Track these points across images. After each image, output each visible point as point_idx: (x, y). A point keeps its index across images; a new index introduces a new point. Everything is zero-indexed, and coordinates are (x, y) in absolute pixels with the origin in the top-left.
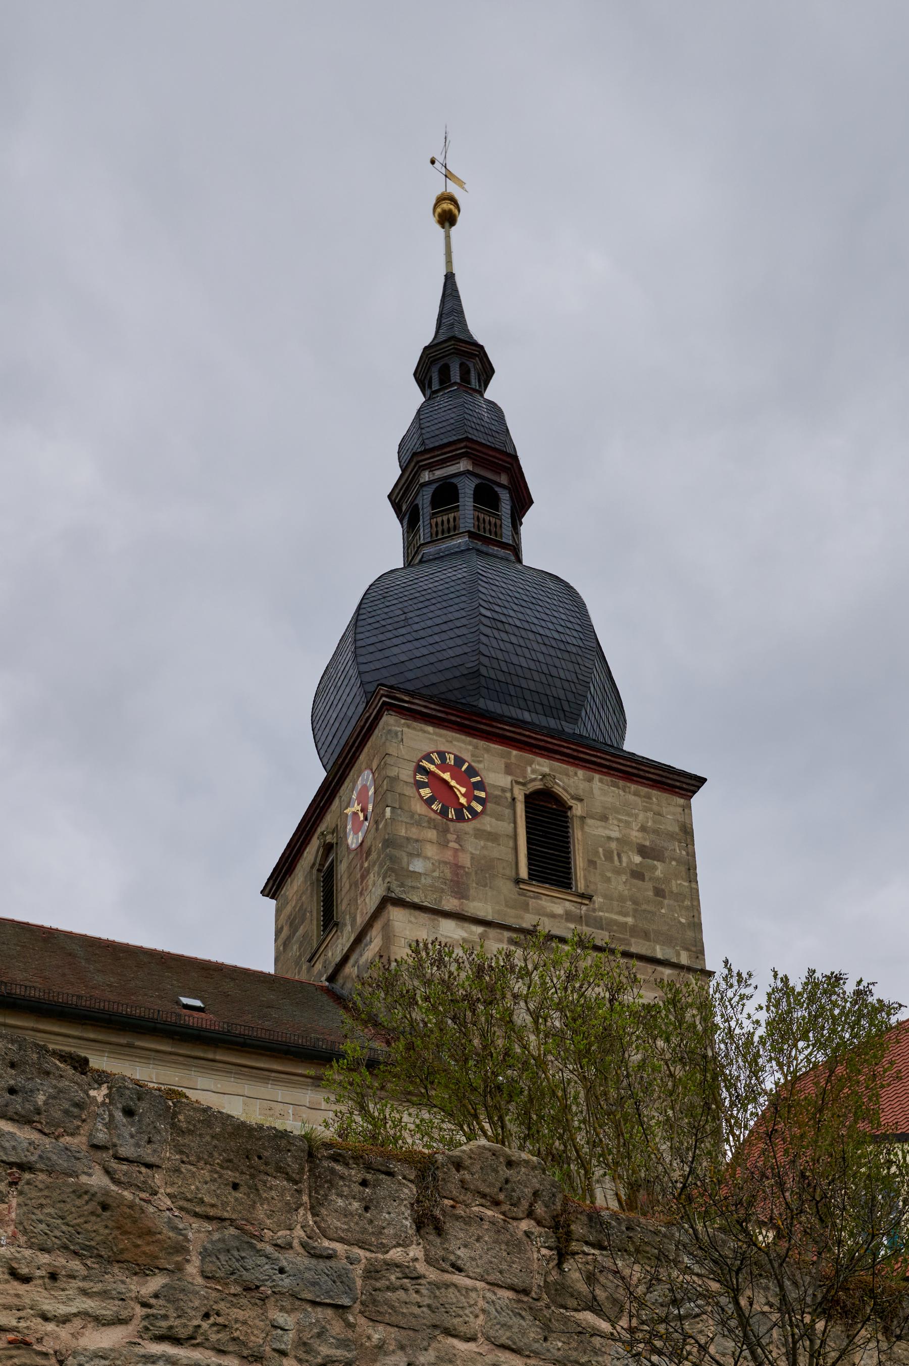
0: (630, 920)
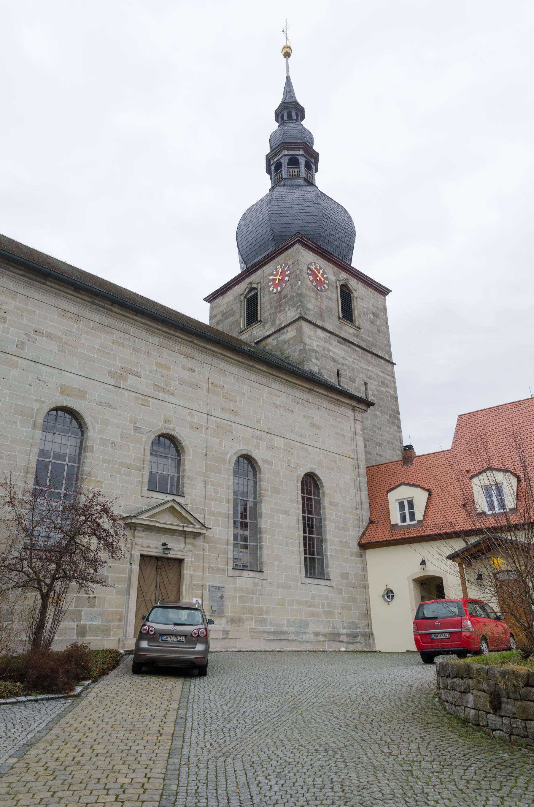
0: (371, 339)
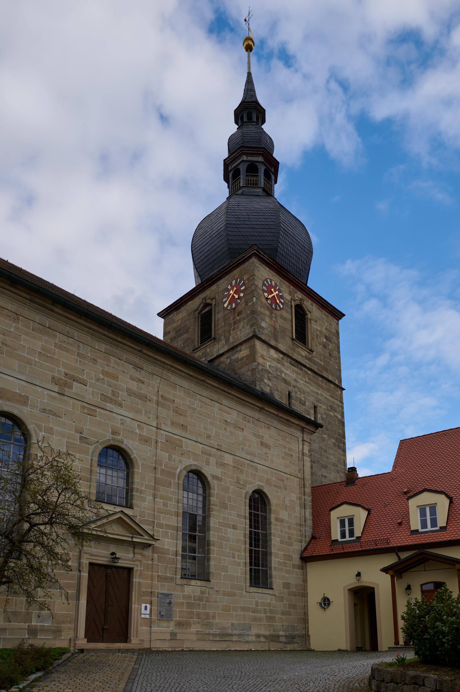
0: (323, 363)
